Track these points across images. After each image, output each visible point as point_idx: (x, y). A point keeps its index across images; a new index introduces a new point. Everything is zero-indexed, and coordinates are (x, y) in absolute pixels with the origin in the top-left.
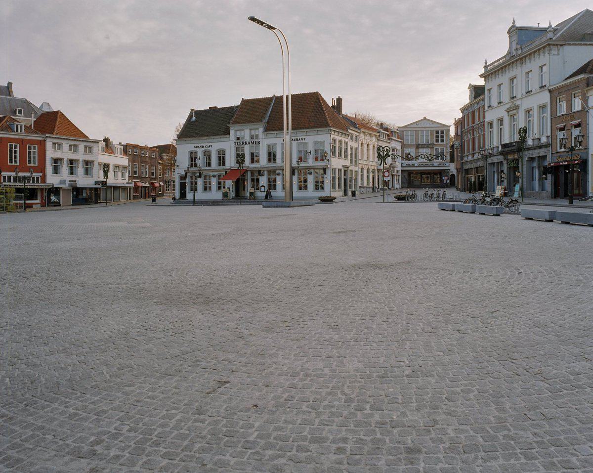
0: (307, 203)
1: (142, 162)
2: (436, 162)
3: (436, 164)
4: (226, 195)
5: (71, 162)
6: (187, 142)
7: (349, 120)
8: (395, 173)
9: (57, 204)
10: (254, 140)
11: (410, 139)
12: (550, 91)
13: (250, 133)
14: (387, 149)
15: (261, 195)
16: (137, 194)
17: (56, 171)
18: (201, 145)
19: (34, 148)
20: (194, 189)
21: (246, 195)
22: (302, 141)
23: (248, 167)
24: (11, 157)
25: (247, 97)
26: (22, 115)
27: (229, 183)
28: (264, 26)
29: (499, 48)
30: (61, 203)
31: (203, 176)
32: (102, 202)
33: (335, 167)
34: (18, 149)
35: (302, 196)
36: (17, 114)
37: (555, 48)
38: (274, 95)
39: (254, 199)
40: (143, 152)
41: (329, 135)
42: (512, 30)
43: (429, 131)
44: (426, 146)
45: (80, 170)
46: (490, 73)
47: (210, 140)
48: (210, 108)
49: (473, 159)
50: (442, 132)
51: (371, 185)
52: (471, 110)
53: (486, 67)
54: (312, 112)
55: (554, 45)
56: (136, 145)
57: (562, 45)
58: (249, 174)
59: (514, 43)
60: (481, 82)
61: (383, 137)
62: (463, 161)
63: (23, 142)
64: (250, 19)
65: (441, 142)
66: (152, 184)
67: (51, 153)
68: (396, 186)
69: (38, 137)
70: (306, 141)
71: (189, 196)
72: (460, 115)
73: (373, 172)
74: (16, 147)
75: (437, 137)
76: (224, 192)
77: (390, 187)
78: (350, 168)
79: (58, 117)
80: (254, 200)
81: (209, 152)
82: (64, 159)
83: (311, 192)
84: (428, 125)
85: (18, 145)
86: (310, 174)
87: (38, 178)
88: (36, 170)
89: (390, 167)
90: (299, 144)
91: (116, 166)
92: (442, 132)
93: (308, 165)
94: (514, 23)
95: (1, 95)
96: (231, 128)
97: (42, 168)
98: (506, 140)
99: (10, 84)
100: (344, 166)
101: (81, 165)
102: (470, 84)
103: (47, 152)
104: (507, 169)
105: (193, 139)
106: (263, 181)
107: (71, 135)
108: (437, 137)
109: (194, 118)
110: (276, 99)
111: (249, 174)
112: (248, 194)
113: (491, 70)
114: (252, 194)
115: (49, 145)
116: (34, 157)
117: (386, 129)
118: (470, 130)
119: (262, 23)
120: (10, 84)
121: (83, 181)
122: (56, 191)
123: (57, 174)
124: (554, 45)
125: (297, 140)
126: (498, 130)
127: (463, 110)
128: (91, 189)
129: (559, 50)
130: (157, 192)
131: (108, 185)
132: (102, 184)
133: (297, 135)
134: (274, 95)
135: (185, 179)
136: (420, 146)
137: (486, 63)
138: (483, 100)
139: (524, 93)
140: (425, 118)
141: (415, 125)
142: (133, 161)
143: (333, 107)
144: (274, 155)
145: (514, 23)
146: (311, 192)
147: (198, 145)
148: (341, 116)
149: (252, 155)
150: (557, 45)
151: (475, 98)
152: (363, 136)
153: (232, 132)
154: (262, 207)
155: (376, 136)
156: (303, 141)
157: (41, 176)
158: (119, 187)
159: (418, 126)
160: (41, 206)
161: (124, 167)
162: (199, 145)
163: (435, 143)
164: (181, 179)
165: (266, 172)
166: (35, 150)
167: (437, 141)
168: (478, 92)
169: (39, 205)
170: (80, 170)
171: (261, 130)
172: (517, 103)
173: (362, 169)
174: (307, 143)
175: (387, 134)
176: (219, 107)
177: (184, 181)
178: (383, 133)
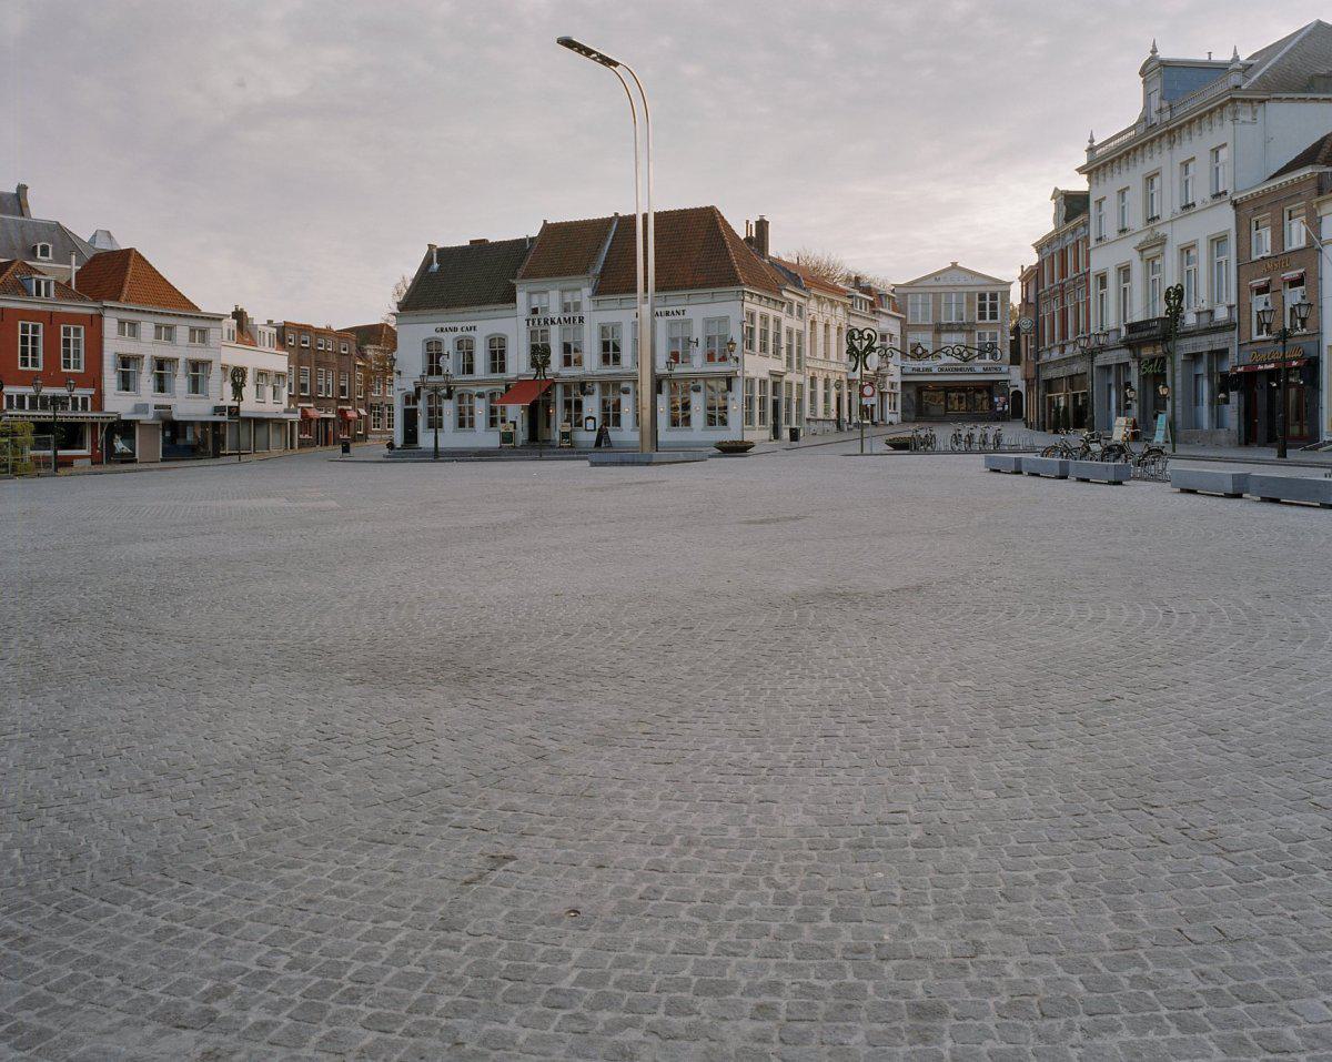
0: (689, 455)
1: (319, 364)
2: (980, 364)
3: (979, 369)
4: (507, 438)
5: (161, 363)
6: (421, 319)
7: (784, 269)
8: (887, 389)
9: (128, 459)
10: (571, 315)
11: (920, 313)
12: (1235, 205)
13: (562, 298)
14: (869, 335)
15: (586, 437)
16: (307, 436)
17: (126, 383)
18: (452, 325)
19: (77, 331)
20: (435, 424)
21: (553, 438)
22: (677, 317)
23: (557, 375)
24: (24, 352)
25: (555, 218)
26: (50, 258)
27: (515, 412)
28: (594, 59)
29: (1121, 107)
30: (137, 456)
31: (455, 396)
32: (229, 454)
33: (751, 374)
34: (40, 335)
35: (679, 439)
36: (39, 256)
37: (1247, 107)
38: (616, 214)
39: (571, 447)
40: (321, 341)
41: (740, 303)
42: (1149, 67)
43: (965, 295)
44: (956, 328)
45: (181, 382)
46: (1100, 164)
47: (471, 315)
48: (471, 242)
49: (1062, 357)
50: (994, 296)
51: (834, 416)
52: (1057, 247)
53: (1091, 150)
54: (702, 251)
55: (1244, 101)
56: (305, 326)
57: (1262, 101)
58: (559, 390)
59: (1155, 97)
60: (1081, 184)
61: (861, 308)
62: (1041, 361)
63: (51, 319)
64: (562, 44)
65: (991, 318)
66: (342, 413)
67: (114, 344)
68: (890, 417)
69: (86, 308)
70: (687, 316)
71: (425, 439)
72: (1033, 259)
73: (839, 385)
74: (35, 329)
75: (982, 307)
76: (503, 431)
77: (876, 420)
78: (786, 378)
79: (131, 262)
80: (569, 449)
81: (471, 341)
82: (143, 356)
83: (698, 431)
84: (962, 282)
85: (41, 326)
86: (697, 390)
87: (84, 400)
88: (80, 381)
89: (875, 374)
90: (671, 324)
91: (262, 374)
92: (994, 296)
93: (692, 370)
94: (1154, 51)
95: (3, 213)
96: (518, 288)
97: (94, 378)
98: (1137, 315)
99: (22, 189)
100: (772, 374)
101: (181, 370)
102: (1056, 189)
103: (106, 341)
104: (1139, 379)
105: (433, 311)
106: (592, 406)
107: (159, 304)
108: (982, 307)
109: (436, 266)
110: (619, 221)
111: (559, 390)
112: (557, 437)
113: (1102, 157)
114: (565, 435)
115: (110, 324)
116: (77, 353)
117: (868, 290)
118: (1055, 293)
119: (589, 52)
120: (22, 189)
121: (187, 406)
122: (125, 428)
123: (127, 390)
124: (1244, 101)
125: (667, 314)
126: (1119, 293)
127: (1039, 247)
128: (204, 424)
129: (1255, 112)
130: (352, 432)
131: (242, 415)
132: (230, 413)
133: (668, 303)
134: (616, 214)
135: (415, 403)
136: (944, 328)
137: (1092, 141)
138: (1086, 225)
139: (1178, 209)
140: (954, 265)
141: (932, 282)
142: (299, 362)
143: (749, 240)
144: (616, 348)
145: (1154, 51)
146: (698, 431)
147: (444, 325)
148: (766, 261)
149: (567, 348)
150: (1251, 101)
151: (1067, 219)
152: (815, 305)
153: (521, 297)
154: (588, 464)
155: (844, 305)
156: (681, 317)
157: (91, 396)
158: (268, 420)
159: (940, 283)
160: (93, 464)
161: (279, 375)
162: (447, 325)
163: (978, 321)
164: (407, 403)
165: (597, 387)
166: (78, 337)
167: (982, 316)
168: (1073, 206)
169: (88, 461)
170: (181, 382)
171: (587, 291)
172: (1161, 231)
173: (813, 379)
174: (689, 322)
175: (870, 301)
176: (492, 239)
177: (414, 407)
178: (861, 299)
